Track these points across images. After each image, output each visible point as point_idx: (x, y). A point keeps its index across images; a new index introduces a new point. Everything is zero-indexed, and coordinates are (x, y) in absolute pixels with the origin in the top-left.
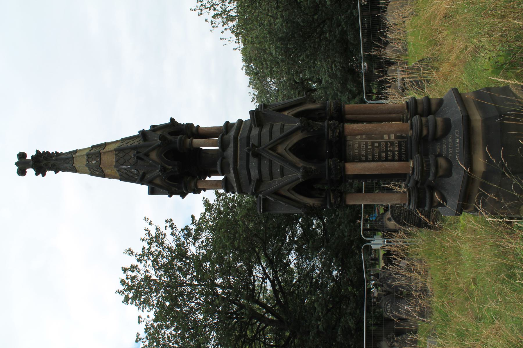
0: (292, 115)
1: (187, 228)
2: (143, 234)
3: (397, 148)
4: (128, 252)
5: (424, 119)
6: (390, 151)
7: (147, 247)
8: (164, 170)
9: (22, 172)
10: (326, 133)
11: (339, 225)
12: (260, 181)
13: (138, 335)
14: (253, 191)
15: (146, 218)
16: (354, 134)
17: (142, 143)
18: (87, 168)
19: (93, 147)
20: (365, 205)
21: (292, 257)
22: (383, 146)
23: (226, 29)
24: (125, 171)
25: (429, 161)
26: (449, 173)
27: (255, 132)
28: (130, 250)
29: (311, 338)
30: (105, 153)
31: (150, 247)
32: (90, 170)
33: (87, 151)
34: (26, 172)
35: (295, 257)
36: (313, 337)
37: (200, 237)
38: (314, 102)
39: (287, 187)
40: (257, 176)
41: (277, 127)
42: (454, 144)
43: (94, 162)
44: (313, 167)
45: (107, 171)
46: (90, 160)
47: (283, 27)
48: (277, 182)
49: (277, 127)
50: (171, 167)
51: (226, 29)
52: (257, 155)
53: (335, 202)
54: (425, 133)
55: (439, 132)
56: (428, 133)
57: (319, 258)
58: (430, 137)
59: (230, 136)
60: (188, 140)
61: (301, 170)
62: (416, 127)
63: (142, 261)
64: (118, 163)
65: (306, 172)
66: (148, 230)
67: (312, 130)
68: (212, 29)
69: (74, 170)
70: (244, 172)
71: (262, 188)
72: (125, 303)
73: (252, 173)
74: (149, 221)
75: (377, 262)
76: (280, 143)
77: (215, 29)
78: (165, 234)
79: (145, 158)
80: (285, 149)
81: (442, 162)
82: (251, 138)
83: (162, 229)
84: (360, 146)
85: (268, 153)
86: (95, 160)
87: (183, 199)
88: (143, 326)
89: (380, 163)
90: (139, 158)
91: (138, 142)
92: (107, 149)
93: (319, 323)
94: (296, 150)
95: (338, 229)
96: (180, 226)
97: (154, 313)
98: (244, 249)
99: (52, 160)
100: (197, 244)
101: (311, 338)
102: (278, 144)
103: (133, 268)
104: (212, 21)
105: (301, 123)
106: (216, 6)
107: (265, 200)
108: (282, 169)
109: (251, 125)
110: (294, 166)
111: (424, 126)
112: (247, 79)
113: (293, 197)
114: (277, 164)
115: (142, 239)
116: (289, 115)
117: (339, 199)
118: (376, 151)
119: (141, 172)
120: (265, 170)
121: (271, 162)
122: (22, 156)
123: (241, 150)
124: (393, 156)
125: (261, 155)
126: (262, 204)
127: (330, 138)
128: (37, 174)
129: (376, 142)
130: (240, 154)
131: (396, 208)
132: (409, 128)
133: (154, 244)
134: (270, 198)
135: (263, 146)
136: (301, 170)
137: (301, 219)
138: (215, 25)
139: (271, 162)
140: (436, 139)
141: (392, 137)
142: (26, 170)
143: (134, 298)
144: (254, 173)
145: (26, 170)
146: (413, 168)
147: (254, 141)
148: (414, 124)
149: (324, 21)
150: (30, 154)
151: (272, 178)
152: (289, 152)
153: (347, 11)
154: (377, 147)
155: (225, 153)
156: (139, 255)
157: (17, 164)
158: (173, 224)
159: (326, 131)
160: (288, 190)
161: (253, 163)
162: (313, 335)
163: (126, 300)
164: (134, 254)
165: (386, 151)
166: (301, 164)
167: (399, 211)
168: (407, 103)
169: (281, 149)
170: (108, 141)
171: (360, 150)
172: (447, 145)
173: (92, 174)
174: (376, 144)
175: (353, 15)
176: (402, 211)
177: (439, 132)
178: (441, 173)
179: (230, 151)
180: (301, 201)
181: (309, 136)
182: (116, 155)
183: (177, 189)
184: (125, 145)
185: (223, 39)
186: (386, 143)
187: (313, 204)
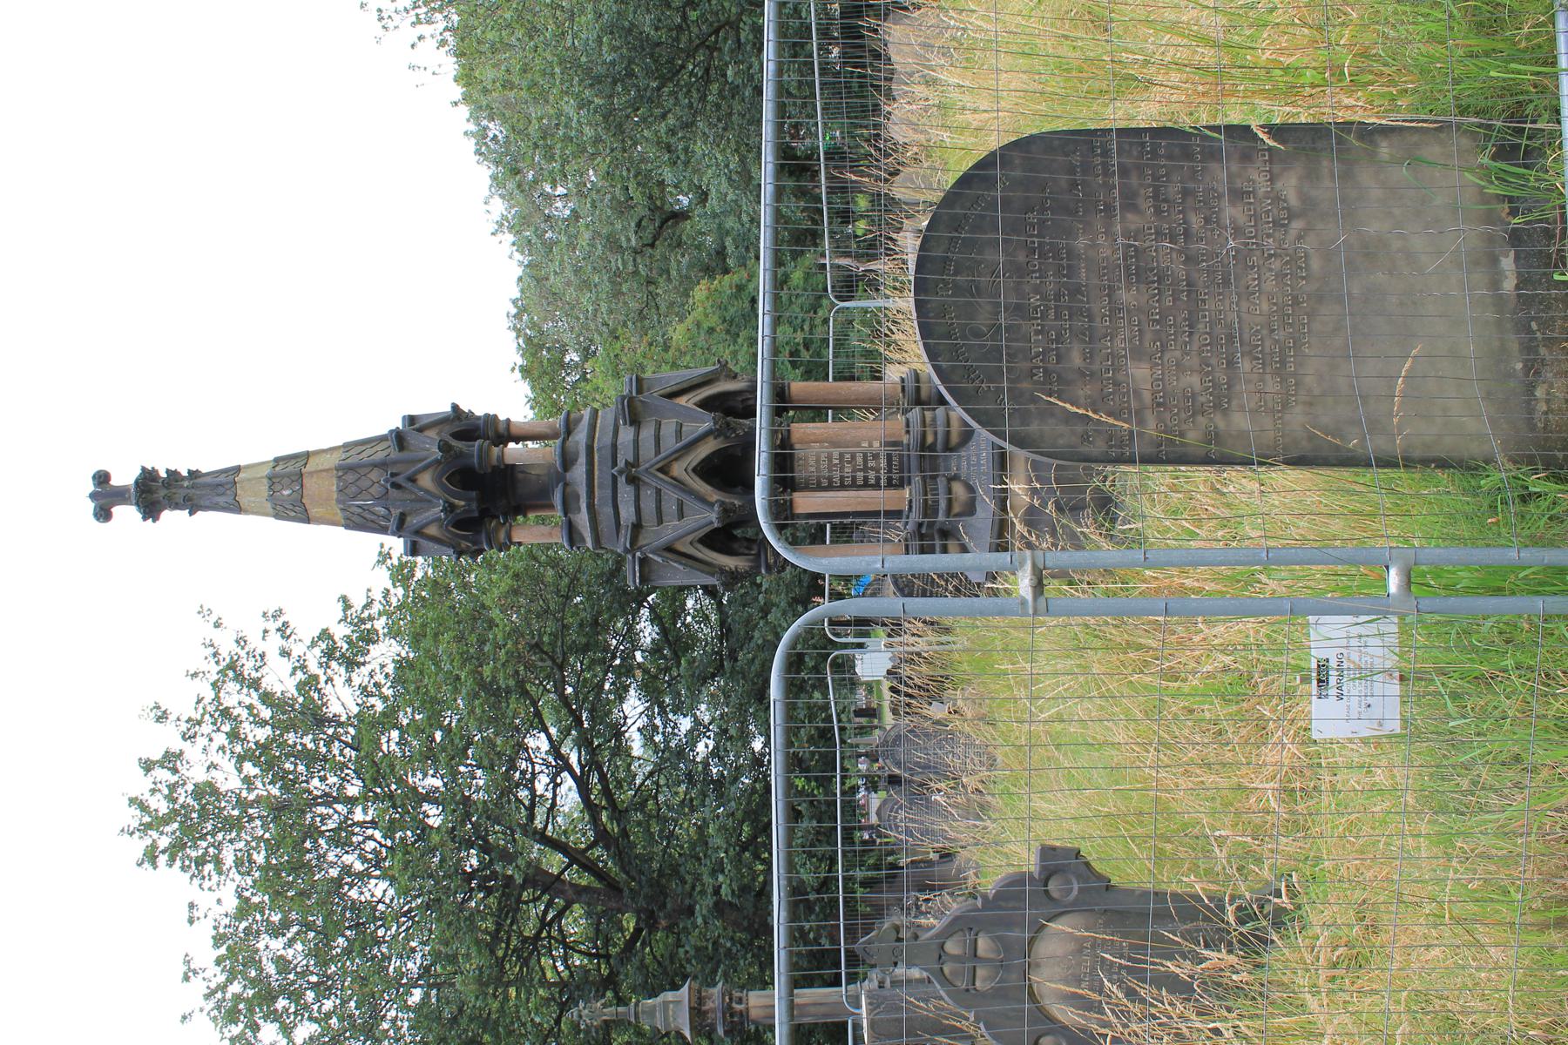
1: (325, 635)
2: (199, 659)
3: (883, 463)
4: (152, 715)
5: (928, 414)
6: (872, 469)
7: (209, 694)
8: (450, 508)
9: (103, 514)
11: (765, 611)
12: (637, 527)
13: (189, 962)
15: (205, 608)
16: (807, 442)
17: (395, 454)
18: (269, 505)
19: (277, 460)
21: (633, 707)
22: (860, 460)
23: (420, 38)
25: (937, 489)
26: (970, 509)
27: (627, 434)
28: (158, 708)
29: (699, 921)
30: (311, 474)
31: (217, 698)
35: (641, 709)
36: (704, 917)
37: (368, 659)
38: (735, 377)
39: (690, 538)
40: (633, 519)
41: (669, 428)
42: (979, 460)
43: (286, 492)
45: (314, 511)
46: (278, 487)
48: (671, 529)
49: (669, 428)
50: (463, 503)
52: (633, 480)
54: (930, 439)
55: (955, 439)
56: (936, 439)
58: (939, 446)
59: (577, 442)
60: (495, 450)
61: (716, 508)
62: (916, 428)
63: (194, 737)
64: (346, 494)
65: (726, 510)
66: (212, 645)
68: (382, 31)
69: (236, 508)
70: (608, 510)
71: (642, 542)
72: (146, 865)
74: (213, 618)
75: (876, 722)
76: (676, 459)
77: (391, 33)
78: (263, 656)
79: (408, 485)
81: (959, 489)
83: (255, 642)
84: (818, 461)
88: (205, 930)
89: (852, 494)
90: (396, 486)
91: (385, 453)
93: (721, 878)
94: (706, 471)
95: (762, 623)
96: (306, 630)
97: (237, 891)
98: (507, 687)
99: (182, 487)
100: (357, 680)
101: (699, 921)
103: (171, 760)
105: (715, 424)
107: (644, 562)
109: (616, 420)
110: (701, 499)
112: (481, 175)
113: (699, 555)
114: (671, 497)
115: (192, 672)
116: (690, 405)
118: (848, 469)
119: (396, 512)
120: (648, 505)
121: (659, 492)
124: (878, 479)
125: (639, 479)
126: (637, 568)
128: (145, 519)
133: (232, 686)
134: (656, 558)
135: (647, 465)
136: (716, 508)
137: (653, 596)
138: (391, 24)
139: (659, 492)
141: (876, 444)
142: (402, 539)
143: (175, 849)
144: (627, 514)
145: (114, 510)
146: (910, 501)
147: (625, 455)
150: (125, 477)
151: (660, 521)
154: (848, 462)
155: (568, 475)
156: (187, 722)
157: (93, 496)
158: (286, 625)
160: (691, 543)
161: (626, 493)
162: (704, 912)
163: (151, 856)
164: (172, 717)
165: (865, 469)
166: (714, 495)
168: (903, 380)
170: (311, 449)
171: (818, 469)
172: (968, 459)
173: (277, 516)
178: (956, 509)
179: (579, 472)
182: (339, 478)
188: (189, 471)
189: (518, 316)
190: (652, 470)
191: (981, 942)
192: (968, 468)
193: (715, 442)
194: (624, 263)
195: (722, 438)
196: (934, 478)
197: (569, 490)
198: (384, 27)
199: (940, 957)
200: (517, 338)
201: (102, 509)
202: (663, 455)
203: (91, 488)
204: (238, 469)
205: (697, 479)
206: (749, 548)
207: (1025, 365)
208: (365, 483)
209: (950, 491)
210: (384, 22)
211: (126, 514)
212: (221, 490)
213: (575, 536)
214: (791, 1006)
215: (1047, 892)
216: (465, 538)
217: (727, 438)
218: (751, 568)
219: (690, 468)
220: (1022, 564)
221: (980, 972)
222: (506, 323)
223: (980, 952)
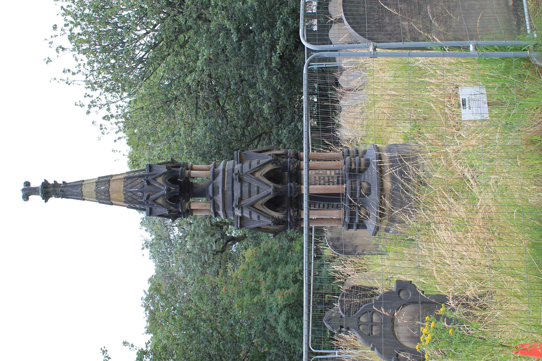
8: (169, 190)
9: (26, 197)
10: (289, 166)
14: (237, 204)
19: (99, 178)
20: (315, 227)
22: (327, 179)
23: (119, 138)
24: (131, 194)
32: (96, 195)
33: (97, 180)
39: (261, 202)
40: (239, 196)
44: (280, 187)
46: (99, 186)
47: (205, 137)
51: (119, 138)
52: (241, 180)
53: (294, 215)
54: (353, 167)
55: (362, 167)
60: (187, 171)
62: (348, 162)
65: (275, 189)
68: (101, 135)
70: (230, 193)
73: (235, 194)
77: (105, 136)
80: (261, 205)
81: (364, 185)
82: (235, 170)
85: (249, 176)
86: (104, 185)
92: (113, 178)
94: (268, 176)
102: (255, 172)
104: (101, 125)
106: (106, 107)
108: (258, 188)
113: (264, 211)
117: (296, 213)
119: (146, 195)
120: (246, 189)
121: (250, 184)
123: (227, 178)
126: (239, 221)
127: (291, 169)
130: (227, 181)
132: (343, 164)
138: (106, 131)
139: (250, 184)
140: (361, 172)
144: (237, 194)
145: (29, 197)
146: (346, 188)
148: (346, 161)
149: (260, 136)
150: (36, 183)
152: (263, 177)
153: (290, 124)
154: (322, 179)
159: (289, 164)
161: (237, 185)
166: (272, 184)
167: (349, 305)
169: (258, 175)
170: (113, 174)
174: (322, 177)
175: (298, 129)
176: (352, 306)
177: (362, 167)
179: (220, 178)
180: (270, 214)
184: (131, 175)
185: (116, 152)
186: (328, 176)
187: (278, 217)
188: (64, 182)
189: (147, 300)
190: (248, 174)
191: (374, 318)
192: (368, 177)
193: (272, 166)
194: (209, 259)
195: (274, 164)
196: (355, 181)
197: (214, 185)
198: (102, 133)
200: (146, 310)
201: (26, 195)
202: (252, 169)
203: (22, 187)
204: (83, 181)
206: (284, 211)
207: (373, 21)
208: (135, 183)
209: (361, 184)
210: (102, 131)
212: (76, 187)
213: (215, 205)
214: (308, 189)
215: (399, 297)
216: (172, 206)
217: (277, 164)
218: (284, 217)
219: (262, 175)
220: (370, 45)
221: (374, 328)
222: (141, 302)
223: (374, 320)
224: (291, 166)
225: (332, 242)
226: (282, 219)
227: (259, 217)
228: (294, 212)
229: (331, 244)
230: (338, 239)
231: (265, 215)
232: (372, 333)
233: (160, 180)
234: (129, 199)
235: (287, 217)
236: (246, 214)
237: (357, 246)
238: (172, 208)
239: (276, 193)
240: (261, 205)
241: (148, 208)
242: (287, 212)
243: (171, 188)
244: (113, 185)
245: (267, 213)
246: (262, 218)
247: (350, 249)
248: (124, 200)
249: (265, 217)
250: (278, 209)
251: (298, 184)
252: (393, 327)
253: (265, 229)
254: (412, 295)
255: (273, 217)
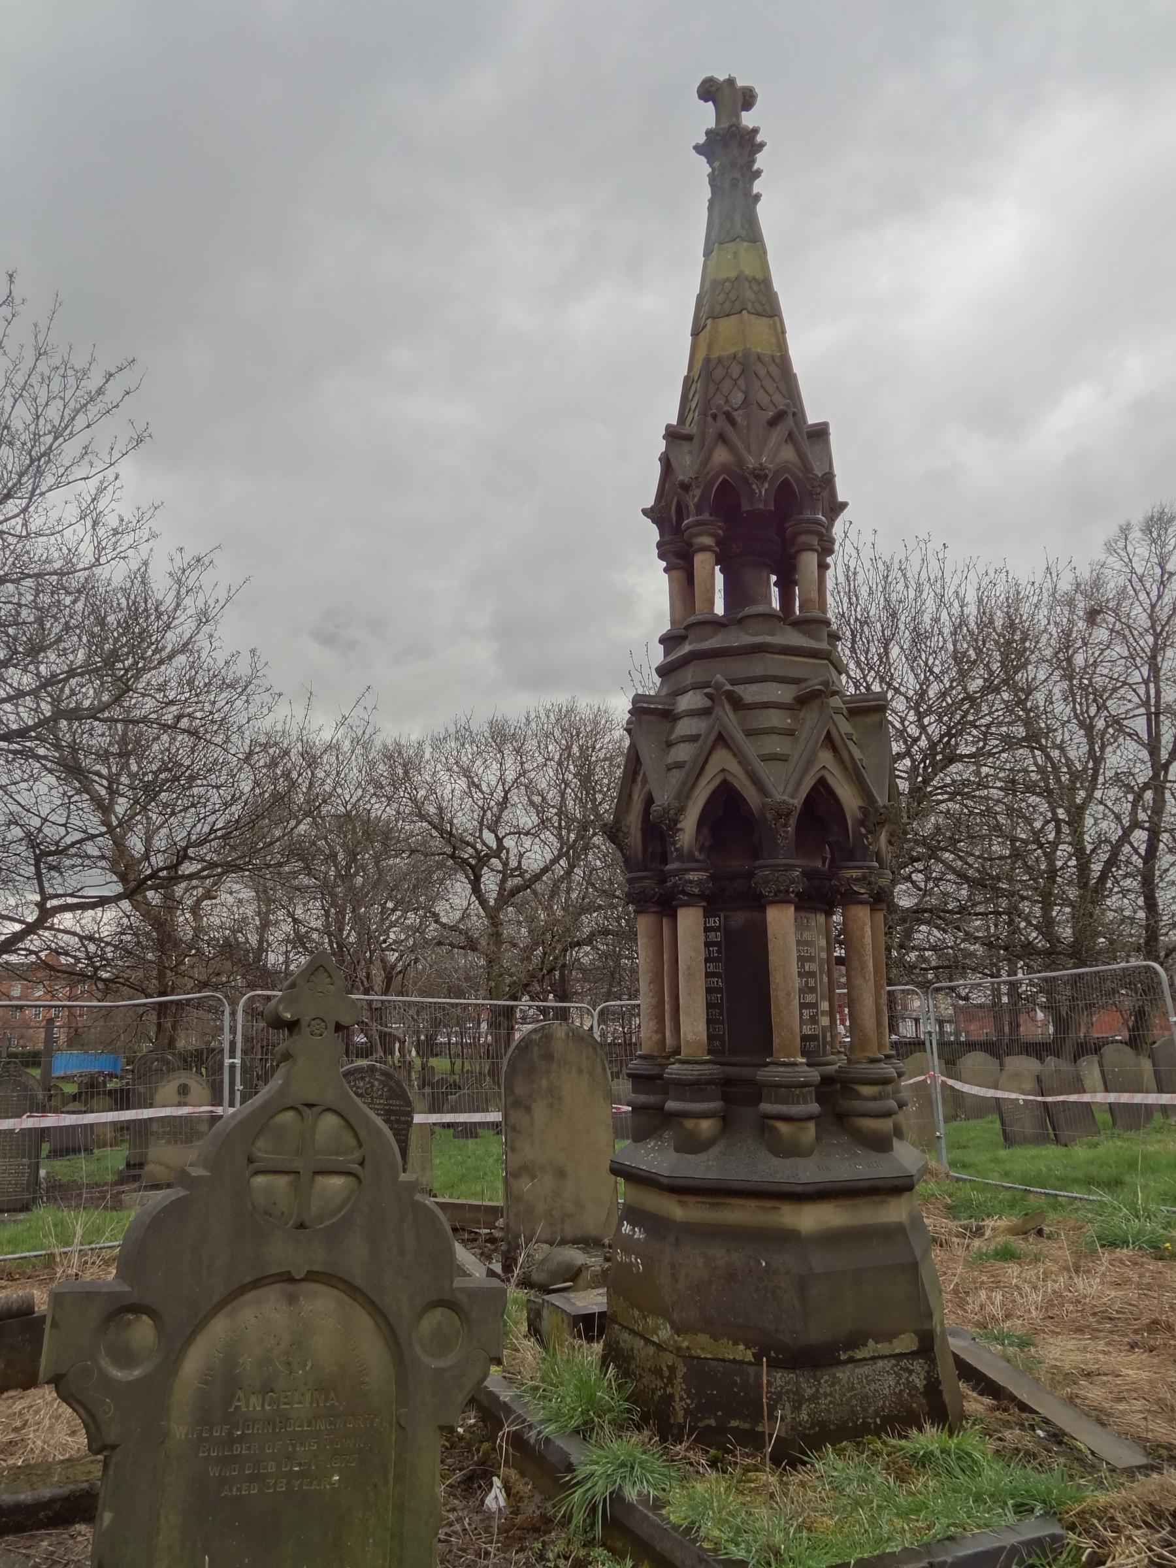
0: (822, 782)
9: (709, 91)
34: (706, 100)
46: (755, 287)
52: (802, 701)
53: (691, 882)
54: (867, 1090)
57: (294, 878)
65: (783, 813)
67: (863, 831)
80: (723, 770)
87: (645, 512)
108: (783, 759)
111: (880, 1087)
113: (703, 781)
120: (776, 719)
122: (747, 99)
129: (816, 982)
131: (369, 1082)
142: (710, 103)
145: (710, 103)
152: (818, 776)
157: (731, 82)
161: (783, 693)
166: (797, 802)
169: (826, 758)
180: (691, 803)
181: (850, 825)
183: (696, 499)
188: (757, 197)
191: (337, 1181)
195: (859, 815)
199: (310, 1106)
205: (813, 782)
206: (701, 850)
211: (706, 116)
217: (862, 823)
223: (321, 1180)
224: (855, 874)
225: (541, 1038)
226: (674, 843)
227: (679, 765)
228: (700, 883)
229: (534, 1037)
230: (548, 1057)
231: (690, 783)
232: (258, 1172)
233: (788, 454)
234: (719, 373)
235: (681, 857)
236: (685, 727)
237: (528, 1110)
238: (697, 492)
239: (769, 816)
240: (723, 770)
241: (686, 430)
242: (697, 861)
243: (766, 485)
244: (760, 325)
245: (697, 791)
246: (676, 777)
247: (520, 1090)
248: (714, 356)
249: (684, 784)
250: (705, 831)
251: (798, 894)
252: (287, 1278)
253: (630, 796)
254: (439, 1372)
255: (682, 810)
